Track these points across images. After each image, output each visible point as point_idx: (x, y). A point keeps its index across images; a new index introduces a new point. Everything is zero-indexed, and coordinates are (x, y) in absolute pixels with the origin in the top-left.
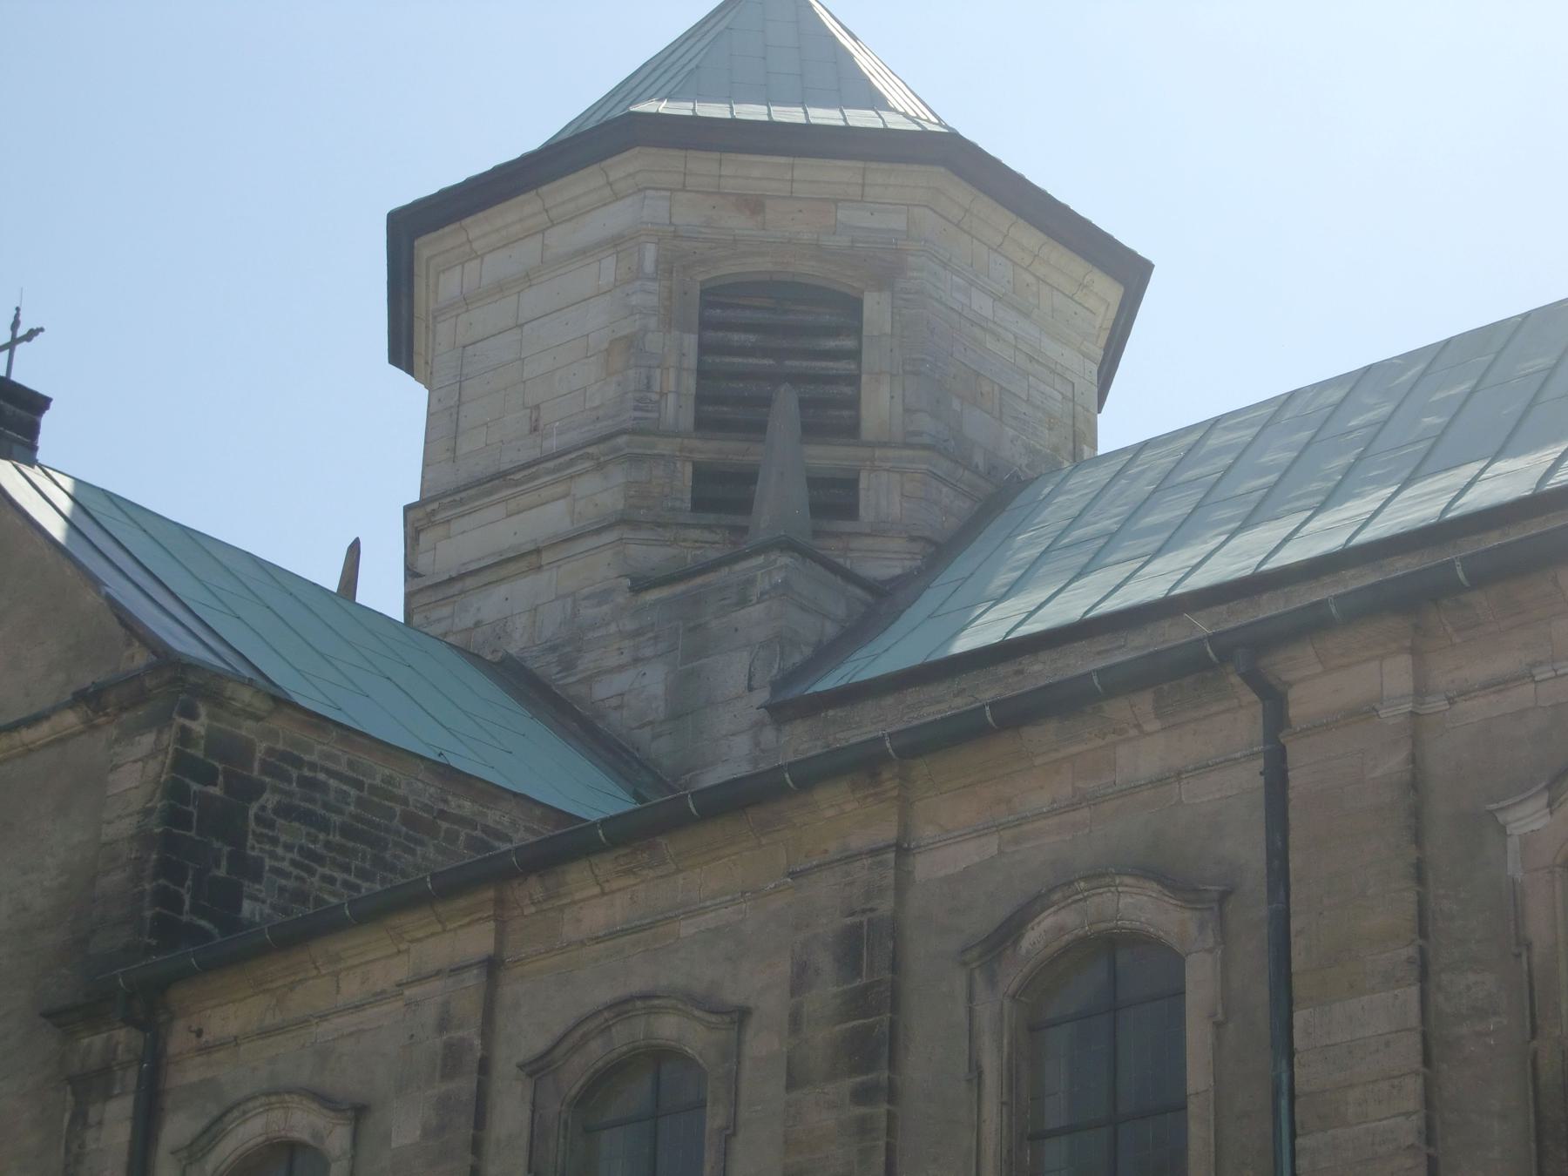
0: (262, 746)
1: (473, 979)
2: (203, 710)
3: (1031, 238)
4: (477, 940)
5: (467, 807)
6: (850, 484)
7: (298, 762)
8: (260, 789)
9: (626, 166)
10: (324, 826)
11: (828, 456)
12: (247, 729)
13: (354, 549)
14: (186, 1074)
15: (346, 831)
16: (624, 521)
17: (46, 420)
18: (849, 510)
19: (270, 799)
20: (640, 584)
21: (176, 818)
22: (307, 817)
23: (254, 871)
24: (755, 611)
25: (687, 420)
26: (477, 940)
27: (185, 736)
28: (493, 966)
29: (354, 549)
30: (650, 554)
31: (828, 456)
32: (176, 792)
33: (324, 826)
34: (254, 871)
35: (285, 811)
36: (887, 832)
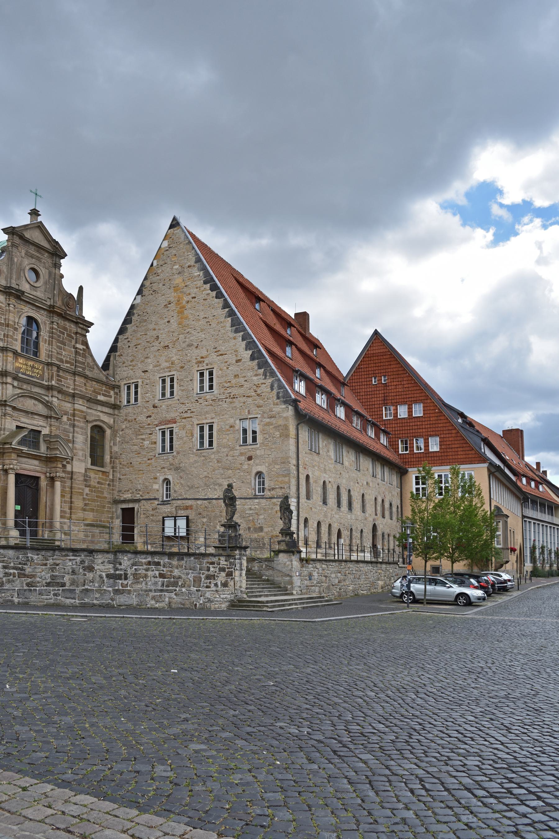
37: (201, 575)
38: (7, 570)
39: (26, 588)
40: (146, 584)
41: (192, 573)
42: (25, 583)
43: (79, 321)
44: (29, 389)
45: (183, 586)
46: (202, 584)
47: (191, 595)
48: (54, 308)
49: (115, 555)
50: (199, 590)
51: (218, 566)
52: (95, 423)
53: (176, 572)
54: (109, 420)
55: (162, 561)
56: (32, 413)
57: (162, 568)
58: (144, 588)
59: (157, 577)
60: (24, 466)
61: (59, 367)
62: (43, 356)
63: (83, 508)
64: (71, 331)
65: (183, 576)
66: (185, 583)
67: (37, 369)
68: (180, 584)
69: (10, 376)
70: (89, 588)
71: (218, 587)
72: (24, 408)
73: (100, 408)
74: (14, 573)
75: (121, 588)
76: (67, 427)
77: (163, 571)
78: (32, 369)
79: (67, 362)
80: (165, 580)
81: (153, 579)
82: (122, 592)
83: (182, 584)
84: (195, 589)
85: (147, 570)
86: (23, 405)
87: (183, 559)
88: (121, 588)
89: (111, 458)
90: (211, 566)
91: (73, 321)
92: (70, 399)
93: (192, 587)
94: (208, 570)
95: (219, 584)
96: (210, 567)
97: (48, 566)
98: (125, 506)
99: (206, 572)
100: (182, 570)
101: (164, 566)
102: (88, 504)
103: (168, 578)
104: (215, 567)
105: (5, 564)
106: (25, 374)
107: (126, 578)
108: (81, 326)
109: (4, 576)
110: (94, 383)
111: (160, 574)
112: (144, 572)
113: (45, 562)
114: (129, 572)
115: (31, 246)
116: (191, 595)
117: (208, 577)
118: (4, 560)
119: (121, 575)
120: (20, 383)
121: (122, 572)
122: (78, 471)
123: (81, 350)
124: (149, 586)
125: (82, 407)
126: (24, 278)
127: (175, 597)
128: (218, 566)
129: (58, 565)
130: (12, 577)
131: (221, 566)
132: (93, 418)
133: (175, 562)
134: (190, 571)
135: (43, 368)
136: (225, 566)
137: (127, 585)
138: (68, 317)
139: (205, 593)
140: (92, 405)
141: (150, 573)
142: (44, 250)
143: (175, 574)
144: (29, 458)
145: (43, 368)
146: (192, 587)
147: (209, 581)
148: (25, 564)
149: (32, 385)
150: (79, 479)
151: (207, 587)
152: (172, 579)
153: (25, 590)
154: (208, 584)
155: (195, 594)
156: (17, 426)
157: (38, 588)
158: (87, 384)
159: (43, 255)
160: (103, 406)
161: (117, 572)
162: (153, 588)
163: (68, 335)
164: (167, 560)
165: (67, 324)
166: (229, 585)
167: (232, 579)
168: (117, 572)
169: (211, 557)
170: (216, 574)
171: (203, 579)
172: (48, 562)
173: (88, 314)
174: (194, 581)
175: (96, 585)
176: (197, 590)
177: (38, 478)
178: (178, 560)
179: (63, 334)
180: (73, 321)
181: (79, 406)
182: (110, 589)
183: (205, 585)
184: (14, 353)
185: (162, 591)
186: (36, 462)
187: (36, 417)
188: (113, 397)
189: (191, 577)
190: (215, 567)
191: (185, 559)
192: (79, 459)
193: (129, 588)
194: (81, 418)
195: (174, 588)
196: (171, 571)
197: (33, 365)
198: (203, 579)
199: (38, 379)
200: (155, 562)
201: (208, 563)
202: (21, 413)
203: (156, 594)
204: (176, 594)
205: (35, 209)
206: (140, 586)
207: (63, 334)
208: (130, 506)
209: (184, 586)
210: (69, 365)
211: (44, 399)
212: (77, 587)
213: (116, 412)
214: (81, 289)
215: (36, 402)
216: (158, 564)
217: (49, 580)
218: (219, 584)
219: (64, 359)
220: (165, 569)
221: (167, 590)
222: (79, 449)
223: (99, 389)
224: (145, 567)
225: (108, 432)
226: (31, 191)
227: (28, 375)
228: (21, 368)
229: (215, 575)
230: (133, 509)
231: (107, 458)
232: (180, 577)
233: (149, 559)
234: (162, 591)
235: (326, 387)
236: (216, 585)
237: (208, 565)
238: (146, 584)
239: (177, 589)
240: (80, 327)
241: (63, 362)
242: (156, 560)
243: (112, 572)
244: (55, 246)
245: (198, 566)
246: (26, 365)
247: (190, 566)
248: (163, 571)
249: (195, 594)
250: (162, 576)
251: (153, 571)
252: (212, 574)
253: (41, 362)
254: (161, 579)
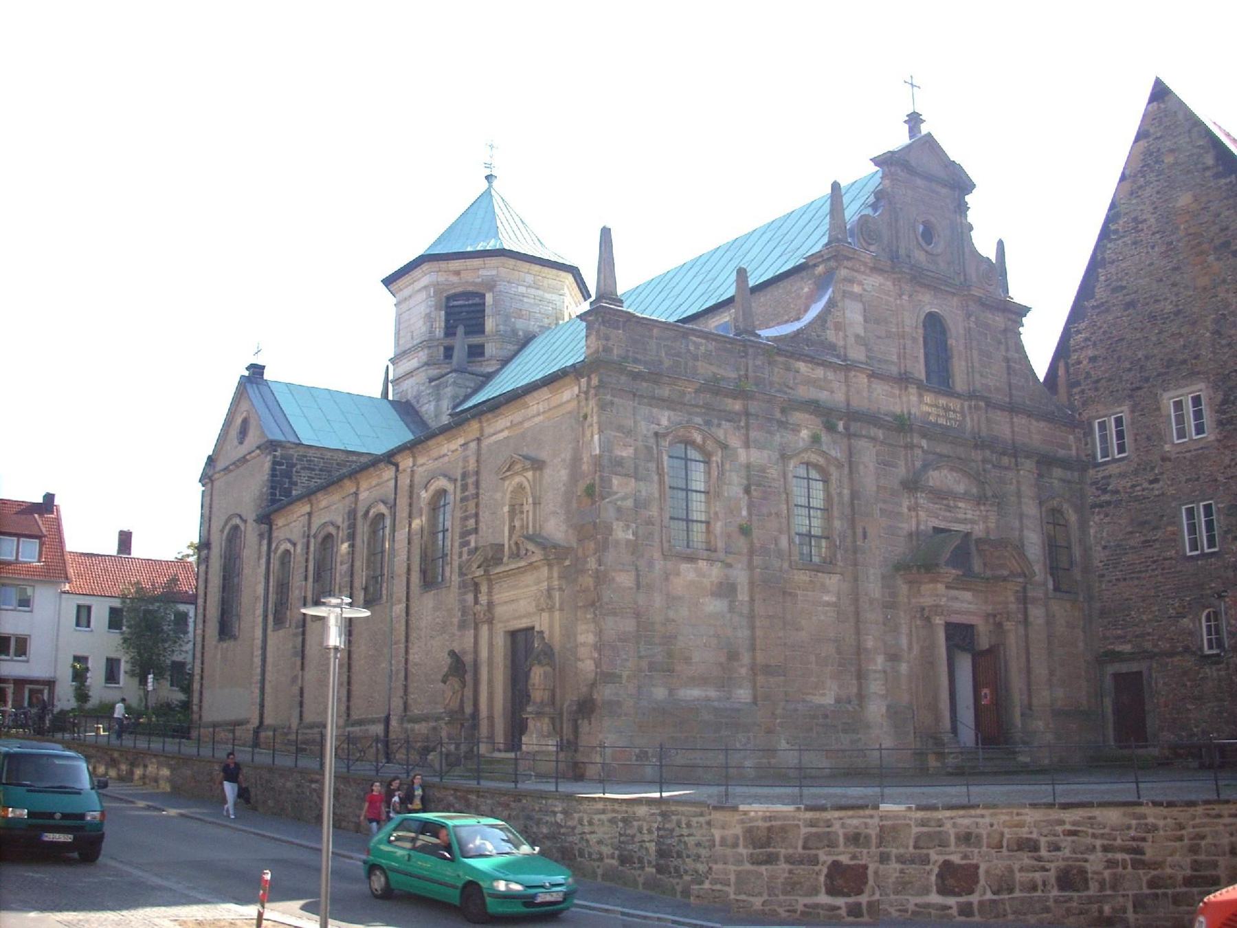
0: (296, 455)
1: (307, 517)
2: (279, 449)
3: (537, 268)
4: (307, 508)
5: (355, 458)
6: (482, 346)
7: (306, 456)
8: (296, 464)
9: (425, 267)
10: (314, 470)
11: (476, 340)
12: (291, 452)
13: (606, 233)
14: (275, 534)
15: (321, 470)
16: (427, 364)
17: (265, 371)
18: (482, 354)
19: (299, 467)
20: (431, 380)
21: (273, 475)
22: (309, 469)
23: (296, 484)
24: (449, 389)
25: (442, 335)
26: (307, 508)
27: (275, 456)
28: (310, 514)
29: (606, 233)
30: (434, 372)
31: (476, 340)
32: (273, 469)
33: (314, 470)
34: (296, 484)
35: (303, 468)
36: (354, 490)
38: (1110, 855)
39: (1146, 891)
42: (1145, 879)
62: (960, 384)
74: (1124, 860)
97: (1186, 841)
98: (1124, 668)
105: (1106, 842)
109: (1107, 867)
113: (1179, 833)
118: (1103, 834)
129: (1203, 838)
130: (1120, 869)
148: (1144, 839)
153: (1147, 896)
156: (934, 528)
157: (1170, 891)
172: (1184, 832)
173: (1018, 292)
177: (971, 627)
188: (1074, 448)
205: (914, 113)
208: (1134, 667)
214: (1001, 244)
217: (1189, 872)
230: (1140, 673)
235: (949, 321)
253: (958, 396)
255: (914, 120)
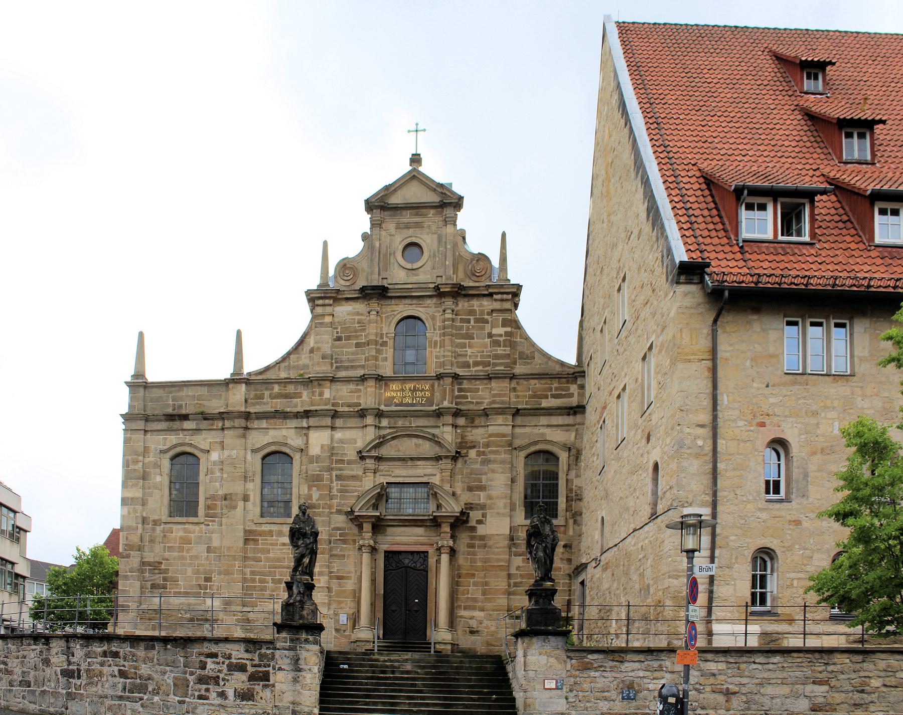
37: (187, 676)
40: (103, 686)
41: (171, 671)
43: (491, 290)
44: (407, 424)
45: (156, 692)
46: (190, 692)
47: (168, 709)
48: (439, 289)
49: (67, 641)
50: (184, 702)
51: (227, 662)
52: (533, 449)
53: (144, 670)
54: (558, 436)
55: (122, 650)
56: (412, 459)
57: (122, 662)
58: (100, 692)
59: (115, 676)
60: (398, 539)
61: (456, 377)
63: (506, 590)
64: (482, 313)
65: (155, 676)
66: (159, 688)
67: (423, 390)
68: (150, 689)
69: (370, 415)
70: (47, 689)
71: (226, 698)
72: (401, 455)
73: (544, 420)
75: (74, 691)
76: (478, 466)
77: (124, 666)
78: (412, 394)
79: (476, 364)
80: (128, 681)
81: (110, 678)
82: (73, 696)
83: (154, 690)
84: (177, 698)
85: (102, 664)
86: (399, 451)
87: (153, 648)
88: (74, 691)
89: (568, 498)
90: (209, 660)
91: (484, 295)
92: (328, 421)
93: (172, 696)
94: (203, 666)
95: (230, 693)
96: (206, 663)
99: (199, 672)
100: (154, 666)
101: (125, 659)
102: (521, 582)
103: (132, 678)
104: (218, 663)
106: (401, 404)
107: (79, 678)
108: (499, 297)
110: (533, 382)
111: (120, 671)
112: (98, 667)
114: (83, 667)
115: (404, 212)
116: (168, 709)
117: (201, 680)
119: (73, 671)
120: (392, 420)
121: (75, 668)
122: (495, 533)
123: (501, 335)
124: (106, 690)
125: (503, 427)
126: (396, 265)
127: (141, 709)
128: (227, 662)
131: (233, 661)
132: (526, 441)
133: (141, 652)
134: (168, 668)
135: (432, 386)
136: (248, 662)
137: (80, 686)
138: (471, 292)
139: (195, 708)
140: (176, 424)
141: (106, 669)
142: (426, 207)
143: (142, 671)
144: (406, 526)
145: (432, 386)
146: (172, 696)
147: (204, 687)
149: (412, 417)
150: (498, 545)
151: (200, 697)
152: (138, 681)
154: (203, 693)
155: (175, 708)
158: (519, 388)
159: (425, 215)
160: (551, 415)
161: (71, 667)
162: (111, 692)
163: (477, 321)
164: (129, 649)
165: (475, 303)
166: (257, 698)
167: (265, 686)
168: (71, 667)
169: (206, 644)
170: (222, 676)
171: (192, 683)
174: (175, 685)
175: (53, 686)
176: (180, 702)
178: (145, 649)
179: (468, 321)
180: (484, 295)
181: (497, 428)
182: (64, 692)
183: (197, 694)
184: (376, 379)
185: (121, 698)
186: (420, 531)
187: (419, 463)
189: (169, 679)
190: (218, 663)
191: (157, 648)
192: (498, 513)
193: (82, 692)
194: (500, 446)
195: (141, 695)
196: (136, 668)
197: (415, 387)
198: (192, 683)
199: (422, 405)
200: (111, 652)
201: (202, 654)
202: (396, 463)
203: (114, 702)
204: (142, 706)
206: (94, 689)
207: (468, 321)
209: (158, 693)
210: (480, 368)
211: (429, 433)
212: (39, 688)
213: (578, 418)
215: (420, 441)
216: (116, 655)
218: (230, 693)
219: (471, 361)
220: (126, 664)
221: (128, 697)
222: (498, 498)
223: (544, 390)
224: (100, 659)
225: (563, 456)
226: (417, 124)
227: (407, 405)
228: (394, 398)
229: (218, 677)
231: (562, 502)
232: (149, 678)
233: (105, 648)
234: (121, 698)
236: (222, 695)
237: (202, 658)
238: (103, 686)
239: (145, 697)
240: (496, 300)
241: (469, 366)
242: (114, 649)
243: (66, 667)
244: (442, 193)
245: (182, 659)
246: (403, 390)
247: (166, 660)
248: (124, 666)
249: (175, 708)
250: (123, 674)
251: (110, 666)
252: (211, 674)
254: (122, 680)
255: (416, 159)
